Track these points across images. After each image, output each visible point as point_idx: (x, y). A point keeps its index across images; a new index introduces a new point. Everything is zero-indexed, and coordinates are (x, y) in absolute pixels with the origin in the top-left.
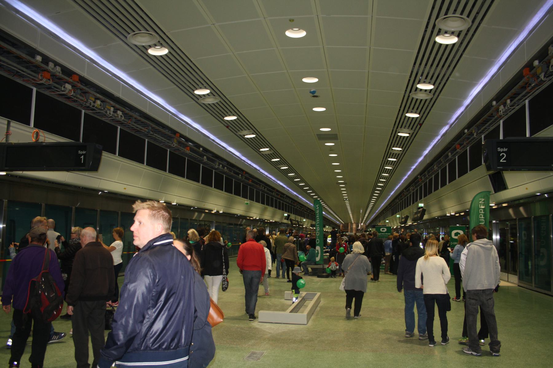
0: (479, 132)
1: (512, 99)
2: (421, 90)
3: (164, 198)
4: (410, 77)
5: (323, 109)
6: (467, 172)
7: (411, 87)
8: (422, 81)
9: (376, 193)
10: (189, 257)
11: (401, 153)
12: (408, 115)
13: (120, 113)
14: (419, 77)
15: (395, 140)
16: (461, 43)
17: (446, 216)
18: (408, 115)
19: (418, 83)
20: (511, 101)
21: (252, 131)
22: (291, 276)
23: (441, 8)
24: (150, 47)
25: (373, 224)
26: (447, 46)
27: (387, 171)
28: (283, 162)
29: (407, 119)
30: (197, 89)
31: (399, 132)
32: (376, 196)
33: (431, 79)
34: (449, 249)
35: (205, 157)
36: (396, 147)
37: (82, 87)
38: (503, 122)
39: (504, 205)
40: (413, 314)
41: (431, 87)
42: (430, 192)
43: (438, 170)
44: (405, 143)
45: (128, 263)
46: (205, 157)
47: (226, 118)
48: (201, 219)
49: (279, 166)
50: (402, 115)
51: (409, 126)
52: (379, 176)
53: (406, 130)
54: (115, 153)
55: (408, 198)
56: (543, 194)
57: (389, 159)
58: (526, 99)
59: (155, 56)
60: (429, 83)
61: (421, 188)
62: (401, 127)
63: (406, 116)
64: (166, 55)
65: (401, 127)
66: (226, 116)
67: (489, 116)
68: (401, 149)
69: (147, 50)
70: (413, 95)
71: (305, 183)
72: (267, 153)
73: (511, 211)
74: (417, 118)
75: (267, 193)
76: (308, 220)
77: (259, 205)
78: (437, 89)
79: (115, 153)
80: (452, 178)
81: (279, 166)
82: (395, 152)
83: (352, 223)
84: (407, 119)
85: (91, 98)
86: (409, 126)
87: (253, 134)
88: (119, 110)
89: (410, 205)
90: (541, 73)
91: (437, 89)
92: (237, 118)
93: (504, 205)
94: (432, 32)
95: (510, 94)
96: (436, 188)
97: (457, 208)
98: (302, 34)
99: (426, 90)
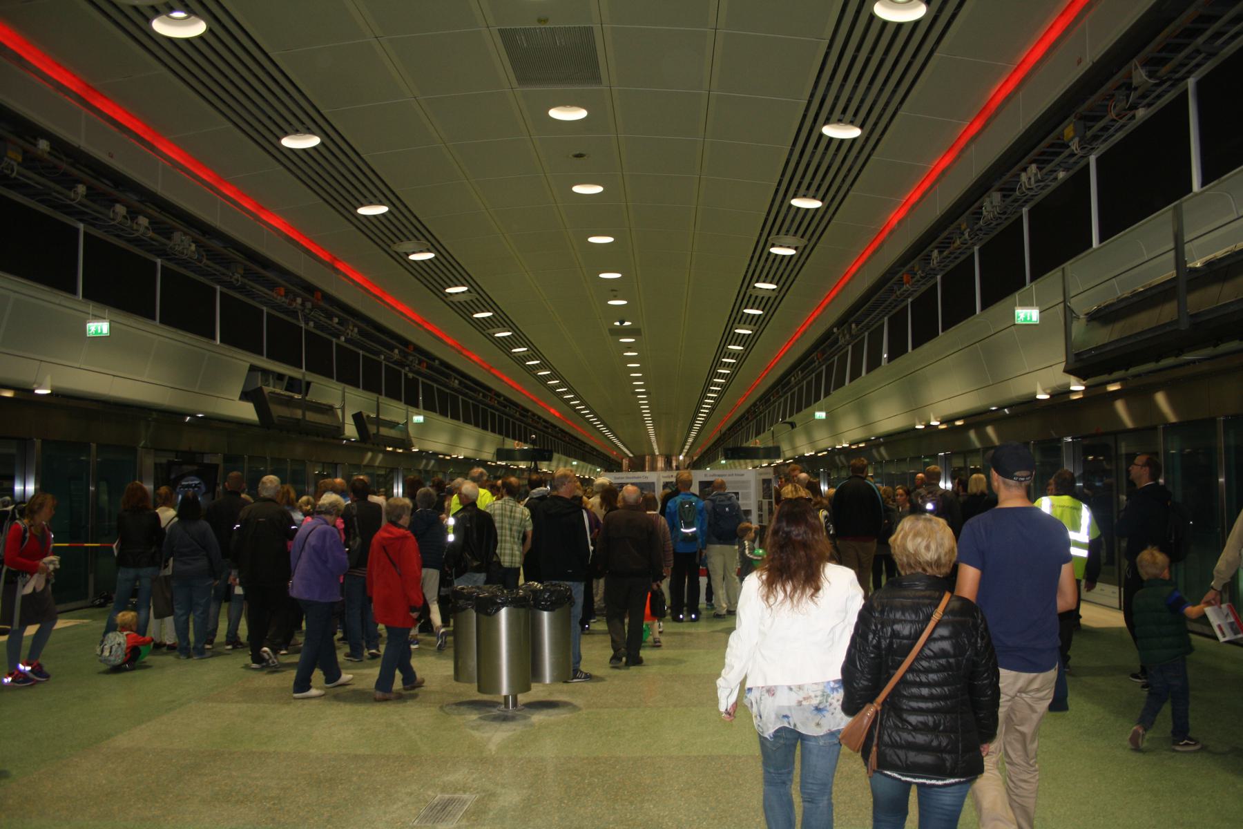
0: (1089, 134)
1: (1153, 64)
3: (48, 380)
4: (783, 175)
5: (598, 189)
6: (1024, 285)
11: (774, 295)
12: (796, 202)
13: (143, 221)
15: (763, 265)
16: (935, 19)
18: (796, 202)
19: (825, 124)
20: (940, 252)
21: (424, 242)
24: (156, 12)
25: (730, 444)
26: (900, 26)
27: (732, 355)
28: (502, 320)
29: (792, 212)
30: (286, 134)
31: (773, 246)
32: (715, 392)
33: (817, 190)
35: (396, 351)
36: (764, 282)
37: (327, 306)
38: (1098, 160)
42: (840, 384)
43: (1085, 156)
44: (784, 271)
46: (396, 351)
47: (363, 211)
48: (377, 464)
49: (491, 331)
50: (782, 202)
51: (796, 232)
52: (722, 351)
53: (789, 239)
54: (73, 291)
55: (801, 389)
56: (1001, 408)
57: (747, 311)
58: (1189, 73)
59: (291, 150)
60: (814, 197)
61: (786, 401)
62: (778, 233)
63: (791, 206)
64: (201, 37)
65: (778, 233)
66: (362, 205)
67: (1052, 145)
68: (773, 286)
69: (149, 21)
71: (550, 369)
72: (462, 298)
73: (972, 434)
74: (817, 210)
75: (465, 395)
76: (582, 463)
77: (447, 422)
78: (828, 208)
79: (73, 291)
80: (897, 351)
81: (491, 331)
83: (653, 454)
84: (792, 212)
85: (10, 154)
87: (429, 251)
88: (118, 201)
89: (874, 363)
90: (1072, 139)
91: (828, 208)
92: (322, 143)
93: (959, 423)
95: (1149, 50)
96: (856, 374)
97: (857, 434)
98: (580, 114)
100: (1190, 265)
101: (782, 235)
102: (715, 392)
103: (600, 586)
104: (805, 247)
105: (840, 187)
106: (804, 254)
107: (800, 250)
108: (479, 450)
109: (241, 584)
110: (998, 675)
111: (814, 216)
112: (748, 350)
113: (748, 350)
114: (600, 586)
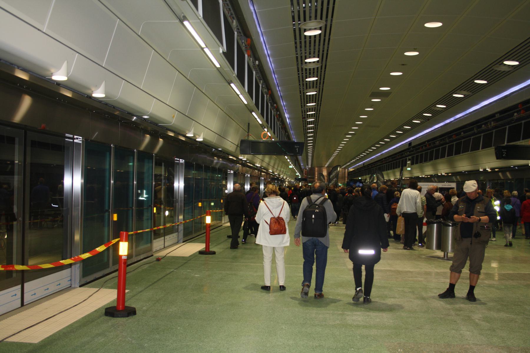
2: (310, 63)
7: (298, 33)
8: (308, 57)
9: (310, 137)
10: (498, 218)
11: (319, 65)
14: (304, 75)
17: (437, 175)
22: (374, 181)
23: (300, 17)
27: (311, 99)
29: (308, 40)
33: (314, 53)
34: (171, 208)
39: (496, 170)
40: (361, 272)
41: (316, 59)
45: (12, 236)
51: (316, 16)
70: (305, 67)
74: (320, 34)
78: (321, 78)
82: (312, 89)
84: (308, 40)
86: (316, 16)
91: (321, 78)
93: (496, 170)
94: (303, 78)
99: (314, 62)
100: (210, 250)
101: (308, 21)
102: (311, 137)
103: (67, 135)
104: (326, 25)
105: (328, 9)
106: (327, 30)
107: (323, 29)
108: (222, 136)
109: (500, 216)
110: (422, 227)
111: (317, 83)
112: (324, 57)
113: (319, 105)
114: (67, 135)
